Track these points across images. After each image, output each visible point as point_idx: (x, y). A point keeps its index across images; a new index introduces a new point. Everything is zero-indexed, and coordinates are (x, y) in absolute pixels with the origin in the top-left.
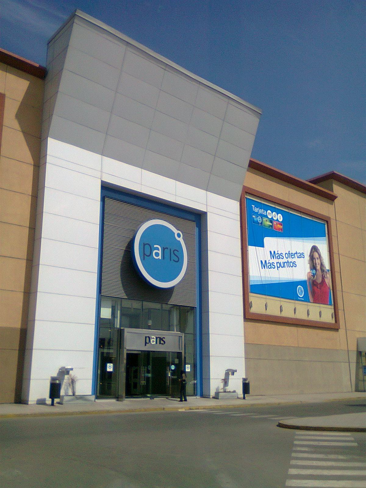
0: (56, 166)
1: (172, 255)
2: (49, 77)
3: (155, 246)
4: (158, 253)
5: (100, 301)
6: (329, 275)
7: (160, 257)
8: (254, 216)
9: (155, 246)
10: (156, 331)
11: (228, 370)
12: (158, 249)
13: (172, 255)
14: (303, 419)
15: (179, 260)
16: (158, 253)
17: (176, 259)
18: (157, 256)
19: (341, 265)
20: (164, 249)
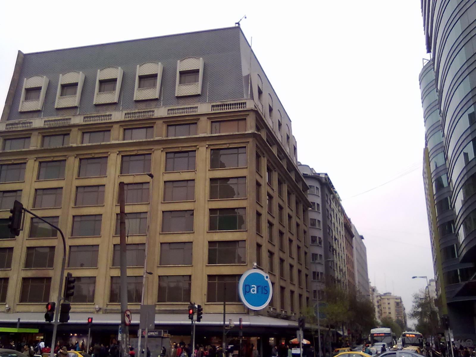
0: (469, 9)
1: (263, 289)
2: (141, 352)
3: (252, 286)
4: (254, 290)
5: (115, 311)
6: (14, 353)
7: (255, 292)
8: (14, 346)
9: (252, 286)
10: (80, 320)
11: (400, 299)
12: (254, 287)
13: (263, 289)
14: (24, 332)
15: (267, 293)
16: (254, 290)
17: (266, 292)
18: (253, 292)
19: (468, 39)
20: (258, 287)
